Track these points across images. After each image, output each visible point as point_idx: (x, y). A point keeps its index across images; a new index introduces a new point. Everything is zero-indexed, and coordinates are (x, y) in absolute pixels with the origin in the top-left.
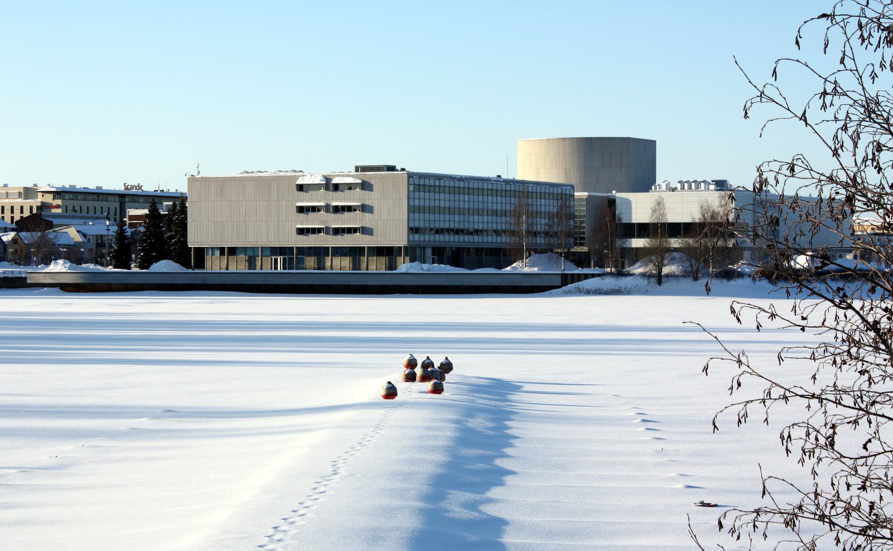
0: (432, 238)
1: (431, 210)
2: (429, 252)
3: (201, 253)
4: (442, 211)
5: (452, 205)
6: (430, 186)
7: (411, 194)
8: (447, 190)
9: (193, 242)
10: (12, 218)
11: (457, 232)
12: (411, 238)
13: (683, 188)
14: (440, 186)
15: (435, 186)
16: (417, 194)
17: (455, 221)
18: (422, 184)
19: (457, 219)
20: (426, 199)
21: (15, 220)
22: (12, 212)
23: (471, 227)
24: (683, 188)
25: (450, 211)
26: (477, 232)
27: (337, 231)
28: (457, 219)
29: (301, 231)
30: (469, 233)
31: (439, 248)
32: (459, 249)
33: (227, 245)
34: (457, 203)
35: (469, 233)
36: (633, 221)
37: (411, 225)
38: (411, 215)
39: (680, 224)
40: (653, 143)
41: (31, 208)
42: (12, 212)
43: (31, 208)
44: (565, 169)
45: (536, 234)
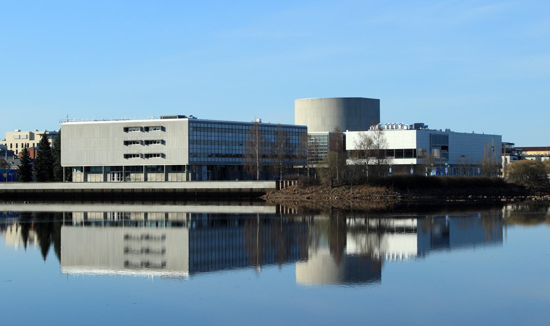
0: (206, 160)
1: (205, 142)
2: (205, 169)
3: (69, 170)
4: (213, 143)
5: (220, 139)
6: (204, 128)
7: (191, 133)
8: (217, 130)
9: (65, 162)
10: (17, 151)
11: (226, 156)
12: (191, 160)
13: (388, 128)
14: (211, 128)
15: (208, 128)
16: (195, 133)
17: (223, 150)
18: (197, 127)
19: (223, 148)
20: (201, 136)
21: (19, 152)
22: (17, 147)
23: (234, 153)
24: (388, 128)
25: (219, 143)
26: (238, 156)
27: (148, 156)
28: (223, 148)
29: (127, 156)
30: (231, 156)
31: (212, 166)
32: (226, 166)
33: (84, 165)
34: (223, 138)
35: (231, 156)
36: (390, 148)
37: (191, 152)
38: (191, 145)
39: (402, 150)
40: (378, 101)
41: (34, 144)
42: (17, 147)
43: (34, 144)
44: (322, 117)
45: (276, 156)
